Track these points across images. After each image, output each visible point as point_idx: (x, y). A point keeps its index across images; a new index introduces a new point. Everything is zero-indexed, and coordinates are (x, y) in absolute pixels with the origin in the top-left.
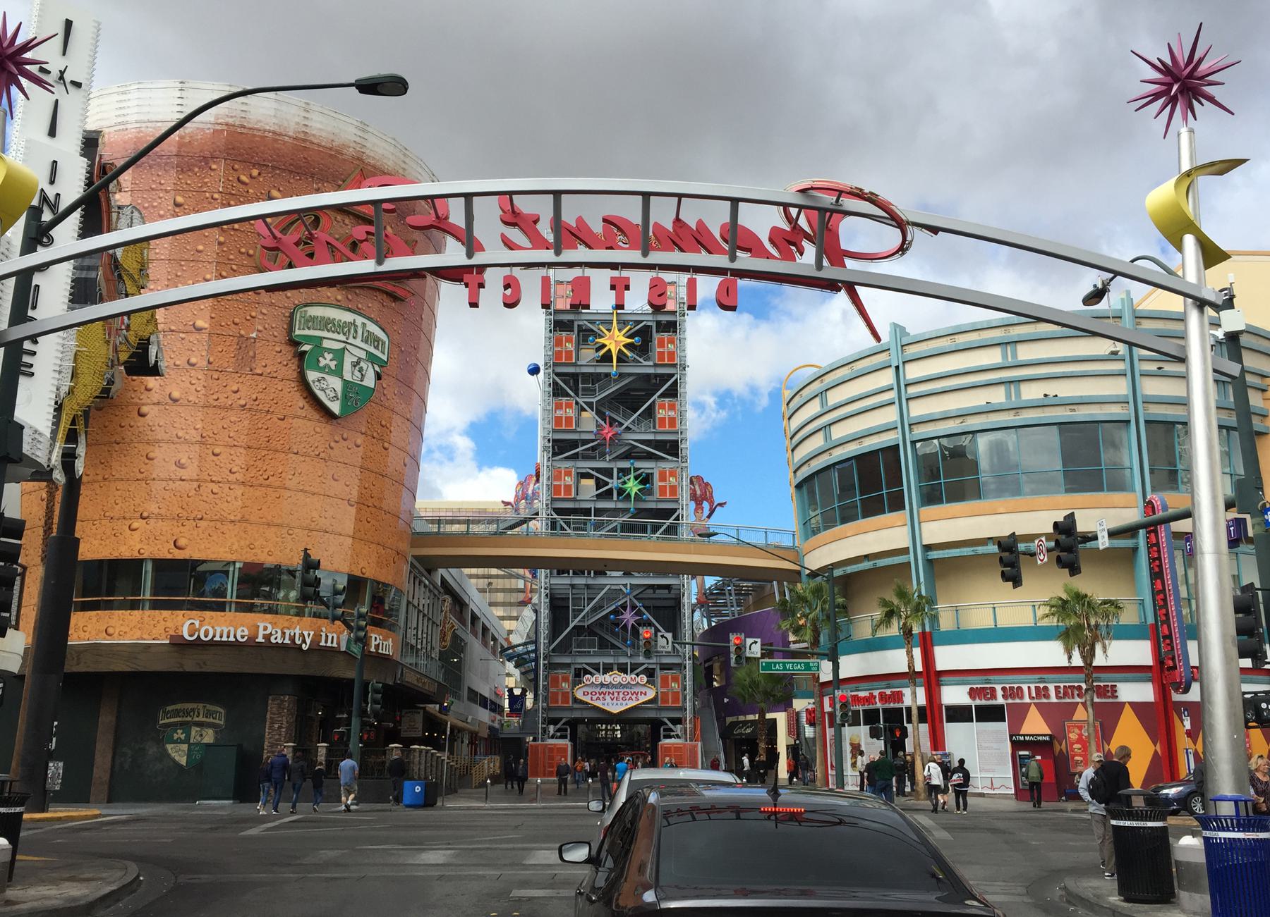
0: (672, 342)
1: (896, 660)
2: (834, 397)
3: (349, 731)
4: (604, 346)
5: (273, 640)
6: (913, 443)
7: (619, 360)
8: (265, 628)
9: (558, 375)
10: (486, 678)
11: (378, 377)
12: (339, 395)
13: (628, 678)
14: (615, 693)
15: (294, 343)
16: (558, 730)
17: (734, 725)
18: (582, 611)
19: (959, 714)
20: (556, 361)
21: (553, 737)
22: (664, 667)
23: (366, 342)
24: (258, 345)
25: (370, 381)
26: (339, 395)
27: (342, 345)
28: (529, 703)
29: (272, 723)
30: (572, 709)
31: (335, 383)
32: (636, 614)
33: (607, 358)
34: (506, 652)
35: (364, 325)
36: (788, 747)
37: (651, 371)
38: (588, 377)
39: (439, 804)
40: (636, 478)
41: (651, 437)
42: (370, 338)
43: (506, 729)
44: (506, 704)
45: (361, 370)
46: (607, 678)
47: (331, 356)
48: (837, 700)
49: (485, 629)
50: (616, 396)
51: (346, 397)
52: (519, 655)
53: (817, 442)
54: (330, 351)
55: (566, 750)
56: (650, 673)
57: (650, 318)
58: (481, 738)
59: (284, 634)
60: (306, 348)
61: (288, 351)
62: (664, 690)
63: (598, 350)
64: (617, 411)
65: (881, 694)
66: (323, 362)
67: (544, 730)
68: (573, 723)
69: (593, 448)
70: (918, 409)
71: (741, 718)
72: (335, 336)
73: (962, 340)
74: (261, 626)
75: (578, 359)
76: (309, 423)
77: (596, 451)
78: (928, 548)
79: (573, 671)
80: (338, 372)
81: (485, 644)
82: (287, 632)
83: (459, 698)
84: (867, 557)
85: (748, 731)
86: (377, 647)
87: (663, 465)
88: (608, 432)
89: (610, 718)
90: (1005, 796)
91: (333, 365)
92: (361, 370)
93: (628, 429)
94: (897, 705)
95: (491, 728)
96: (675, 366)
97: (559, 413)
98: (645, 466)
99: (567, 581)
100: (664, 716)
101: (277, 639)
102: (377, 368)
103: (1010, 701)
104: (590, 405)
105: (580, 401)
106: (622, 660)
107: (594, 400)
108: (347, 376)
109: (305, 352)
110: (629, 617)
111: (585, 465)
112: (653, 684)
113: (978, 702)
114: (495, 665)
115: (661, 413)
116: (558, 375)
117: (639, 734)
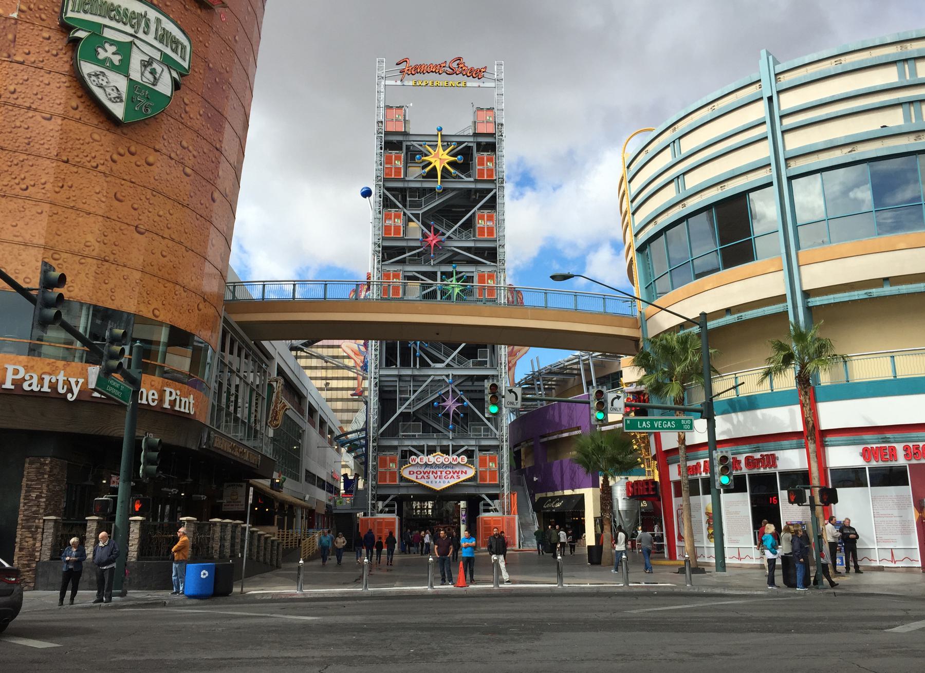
0: (490, 160)
1: (788, 418)
2: (688, 144)
3: (115, 499)
4: (430, 163)
5: (26, 387)
6: (790, 179)
7: (442, 177)
8: (16, 372)
9: (388, 189)
10: (323, 463)
11: (176, 86)
12: (124, 97)
13: (451, 458)
14: (441, 471)
15: (66, 27)
16: (387, 506)
17: (543, 500)
18: (407, 399)
19: (852, 478)
20: (385, 180)
21: (381, 512)
22: (483, 449)
23: (161, 42)
24: (19, 27)
25: (165, 87)
26: (124, 97)
27: (130, 39)
28: (360, 485)
29: (30, 489)
30: (398, 487)
31: (121, 83)
32: (458, 401)
33: (432, 174)
34: (340, 440)
35: (158, 21)
36: (595, 519)
37: (472, 186)
38: (413, 191)
39: (236, 589)
40: (458, 280)
41: (471, 244)
42: (164, 36)
43: (339, 506)
44: (342, 487)
45: (153, 72)
46: (432, 459)
47: (114, 49)
48: (716, 462)
49: (322, 422)
50: (442, 201)
51: (131, 100)
52: (351, 442)
53: (669, 194)
54: (113, 43)
55: (393, 523)
56: (470, 454)
57: (471, 139)
58: (318, 514)
59: (41, 380)
60: (81, 34)
61: (59, 42)
62: (482, 469)
63: (424, 167)
64: (440, 222)
65: (747, 458)
66: (102, 55)
67: (374, 506)
68: (402, 500)
69: (419, 254)
70: (795, 142)
71: (550, 494)
72: (120, 26)
73: (849, 61)
74: (10, 369)
75: (406, 175)
76: (84, 128)
77: (421, 257)
78: (807, 294)
79: (399, 453)
80: (123, 68)
81: (322, 433)
82: (47, 378)
83: (296, 478)
84: (728, 311)
85: (558, 505)
86: (173, 403)
87: (482, 269)
88: (433, 239)
89: (429, 494)
90: (909, 570)
91: (116, 59)
92: (153, 72)
93: (449, 238)
94: (768, 470)
95: (328, 506)
96: (493, 181)
97: (388, 222)
98: (466, 269)
99: (395, 372)
100: (483, 492)
101: (32, 384)
102: (175, 75)
103: (914, 462)
104: (417, 216)
105: (408, 213)
106: (445, 443)
107: (420, 212)
108: (135, 75)
109: (78, 40)
110: (451, 405)
111: (411, 269)
112: (473, 464)
113: (874, 464)
114: (331, 452)
115: (480, 223)
116: (388, 189)
117: (447, 511)
